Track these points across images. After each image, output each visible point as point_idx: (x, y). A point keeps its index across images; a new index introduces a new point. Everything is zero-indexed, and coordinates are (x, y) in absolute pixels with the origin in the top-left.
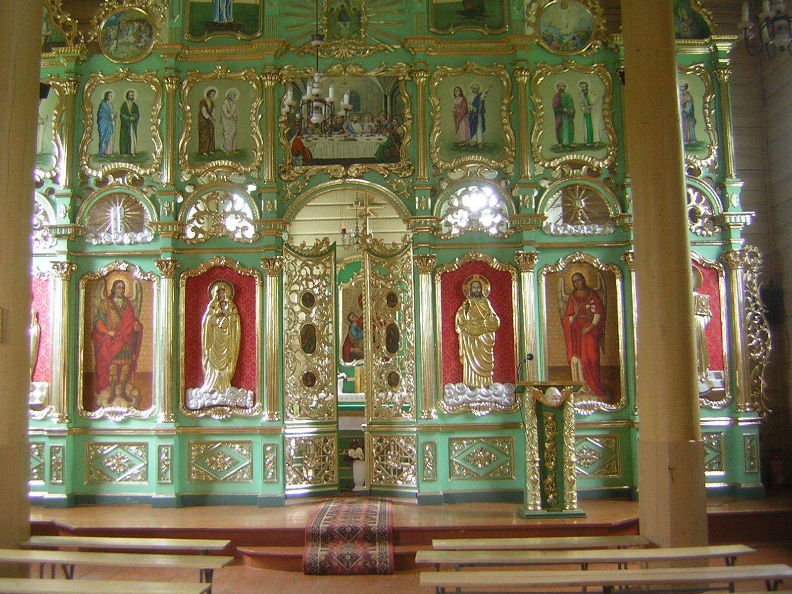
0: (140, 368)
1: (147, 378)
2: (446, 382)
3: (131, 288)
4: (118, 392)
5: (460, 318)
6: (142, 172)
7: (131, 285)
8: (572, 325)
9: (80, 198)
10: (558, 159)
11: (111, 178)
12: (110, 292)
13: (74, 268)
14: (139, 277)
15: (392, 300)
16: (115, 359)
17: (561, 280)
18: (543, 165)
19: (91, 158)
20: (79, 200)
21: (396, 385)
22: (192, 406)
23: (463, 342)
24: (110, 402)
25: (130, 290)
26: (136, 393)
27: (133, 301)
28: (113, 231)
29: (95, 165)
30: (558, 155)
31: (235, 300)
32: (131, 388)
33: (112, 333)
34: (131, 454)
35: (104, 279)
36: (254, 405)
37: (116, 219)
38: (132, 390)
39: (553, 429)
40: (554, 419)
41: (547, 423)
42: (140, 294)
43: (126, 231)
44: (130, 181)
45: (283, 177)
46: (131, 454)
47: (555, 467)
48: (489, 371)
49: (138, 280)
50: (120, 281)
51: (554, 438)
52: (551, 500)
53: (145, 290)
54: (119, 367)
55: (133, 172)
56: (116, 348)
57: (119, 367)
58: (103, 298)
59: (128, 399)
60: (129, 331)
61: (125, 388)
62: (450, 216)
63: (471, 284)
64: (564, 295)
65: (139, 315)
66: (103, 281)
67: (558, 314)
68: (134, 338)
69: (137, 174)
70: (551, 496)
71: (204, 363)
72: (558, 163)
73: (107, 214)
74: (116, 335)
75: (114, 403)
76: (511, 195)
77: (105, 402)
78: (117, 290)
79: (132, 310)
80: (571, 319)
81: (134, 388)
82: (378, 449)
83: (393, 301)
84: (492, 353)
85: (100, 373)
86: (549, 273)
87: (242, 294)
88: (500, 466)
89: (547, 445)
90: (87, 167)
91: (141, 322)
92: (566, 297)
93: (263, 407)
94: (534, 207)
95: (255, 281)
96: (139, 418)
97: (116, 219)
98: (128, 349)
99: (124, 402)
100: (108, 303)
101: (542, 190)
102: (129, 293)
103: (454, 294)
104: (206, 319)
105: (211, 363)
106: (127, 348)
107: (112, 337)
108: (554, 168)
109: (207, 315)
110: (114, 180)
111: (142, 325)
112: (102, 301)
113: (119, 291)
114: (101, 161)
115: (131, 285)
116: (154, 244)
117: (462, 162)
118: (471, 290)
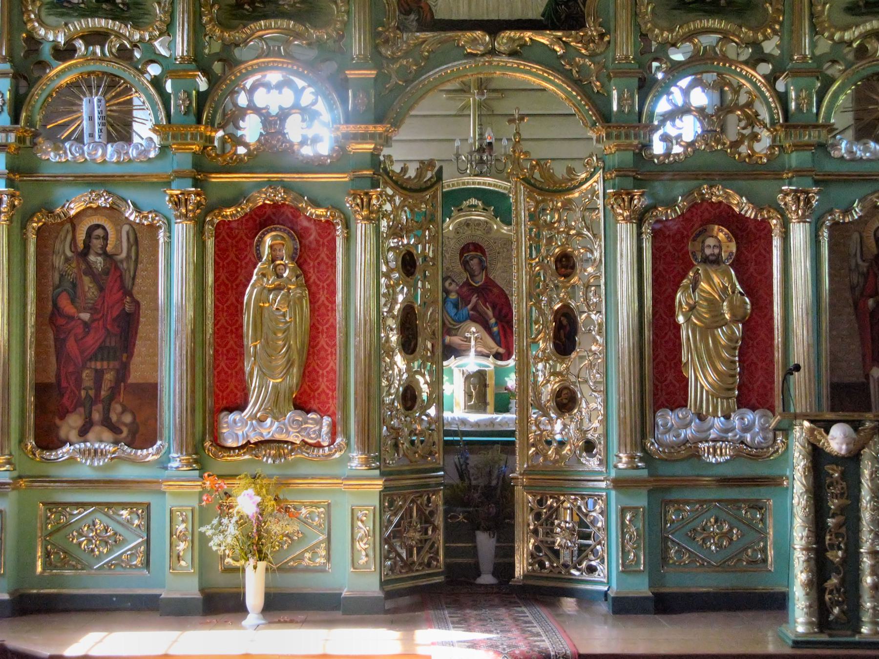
0: (135, 376)
1: (149, 393)
2: (658, 406)
3: (119, 239)
4: (96, 416)
5: (683, 300)
6: (137, 37)
7: (119, 232)
8: (872, 314)
9: (25, 78)
10: (857, 26)
11: (80, 44)
12: (81, 245)
13: (16, 203)
14: (132, 218)
15: (566, 264)
16: (90, 359)
17: (856, 236)
18: (831, 38)
19: (43, 9)
20: (23, 83)
21: (570, 410)
22: (230, 443)
23: (688, 339)
24: (83, 433)
25: (118, 242)
26: (128, 418)
27: (121, 261)
28: (86, 139)
29: (51, 20)
30: (858, 19)
31: (300, 262)
32: (119, 408)
33: (86, 316)
34: (118, 522)
35: (73, 221)
36: (333, 442)
37: (91, 118)
38: (123, 413)
39: (842, 494)
40: (843, 475)
41: (831, 484)
42: (133, 248)
43: (110, 139)
44: (114, 50)
45: (383, 50)
46: (118, 522)
47: (844, 560)
48: (733, 389)
49: (131, 224)
50: (98, 226)
51: (842, 510)
52: (837, 618)
53: (144, 242)
54: (99, 375)
55: (119, 36)
56: (92, 340)
57: (99, 375)
58: (69, 254)
59: (114, 429)
60: (116, 312)
61: (109, 410)
62: (668, 123)
63: (703, 242)
64: (860, 262)
65: (133, 284)
66: (68, 226)
67: (848, 295)
68: (126, 323)
69: (128, 39)
70: (836, 610)
71: (247, 369)
72: (857, 33)
73: (75, 108)
74: (93, 320)
75: (91, 435)
76: (775, 89)
77: (73, 435)
78: (95, 241)
79: (121, 276)
80: (871, 302)
81: (124, 410)
82: (538, 516)
83: (566, 267)
84: (737, 359)
85: (64, 384)
86: (835, 224)
87: (313, 257)
88: (746, 549)
89: (831, 522)
90: (36, 24)
91: (138, 297)
92: (864, 266)
93: (348, 444)
94: (815, 110)
95: (336, 230)
96: (134, 461)
97: (91, 118)
98: (113, 344)
99: (107, 435)
100: (78, 264)
101: (828, 82)
102: (115, 247)
103: (670, 261)
104: (251, 294)
105: (260, 369)
106: (112, 342)
107: (85, 324)
108: (850, 44)
109: (253, 287)
110: (87, 49)
111: (137, 304)
112: (67, 260)
113: (97, 244)
114: (62, 15)
115: (119, 232)
116: (159, 163)
117: (690, 31)
118: (703, 250)
